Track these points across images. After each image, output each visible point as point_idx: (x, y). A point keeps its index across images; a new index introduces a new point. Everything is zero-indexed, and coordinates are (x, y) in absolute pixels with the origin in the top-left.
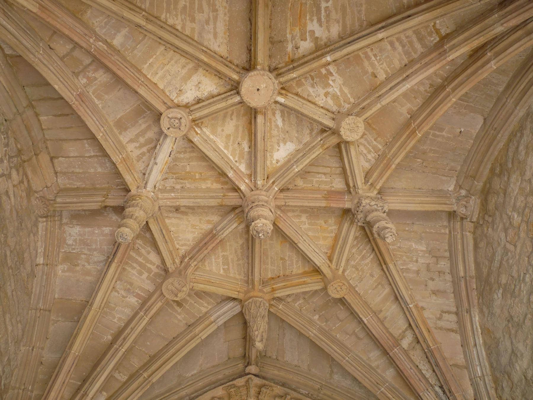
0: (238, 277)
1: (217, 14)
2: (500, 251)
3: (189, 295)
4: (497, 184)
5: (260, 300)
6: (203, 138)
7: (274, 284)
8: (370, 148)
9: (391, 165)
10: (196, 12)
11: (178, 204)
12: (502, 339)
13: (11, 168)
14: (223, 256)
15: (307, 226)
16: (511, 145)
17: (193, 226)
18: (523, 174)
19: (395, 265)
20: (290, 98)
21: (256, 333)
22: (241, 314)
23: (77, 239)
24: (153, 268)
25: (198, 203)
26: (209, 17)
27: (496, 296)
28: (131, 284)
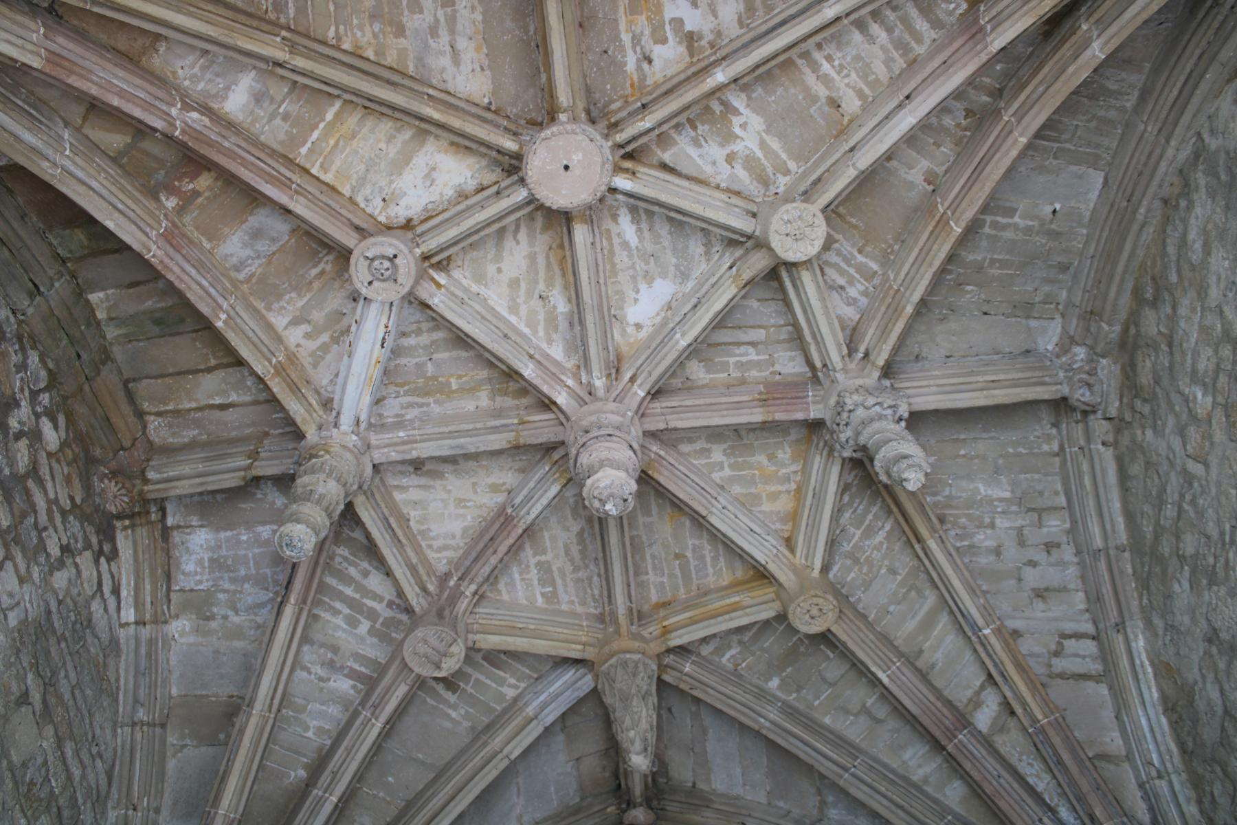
0: (579, 609)
1: (455, 11)
2: (1174, 482)
3: (468, 660)
4: (1152, 323)
5: (636, 657)
6: (453, 294)
7: (665, 618)
8: (852, 271)
9: (904, 308)
10: (406, 13)
11: (415, 454)
12: (1200, 684)
13: (37, 416)
14: (539, 564)
15: (727, 472)
16: (1169, 229)
17: (460, 502)
18: (1202, 293)
19: (943, 542)
20: (645, 177)
21: (632, 734)
22: (595, 693)
23: (202, 558)
24: (379, 607)
25: (461, 447)
26: (437, 21)
27: (1176, 587)
28: (335, 649)
